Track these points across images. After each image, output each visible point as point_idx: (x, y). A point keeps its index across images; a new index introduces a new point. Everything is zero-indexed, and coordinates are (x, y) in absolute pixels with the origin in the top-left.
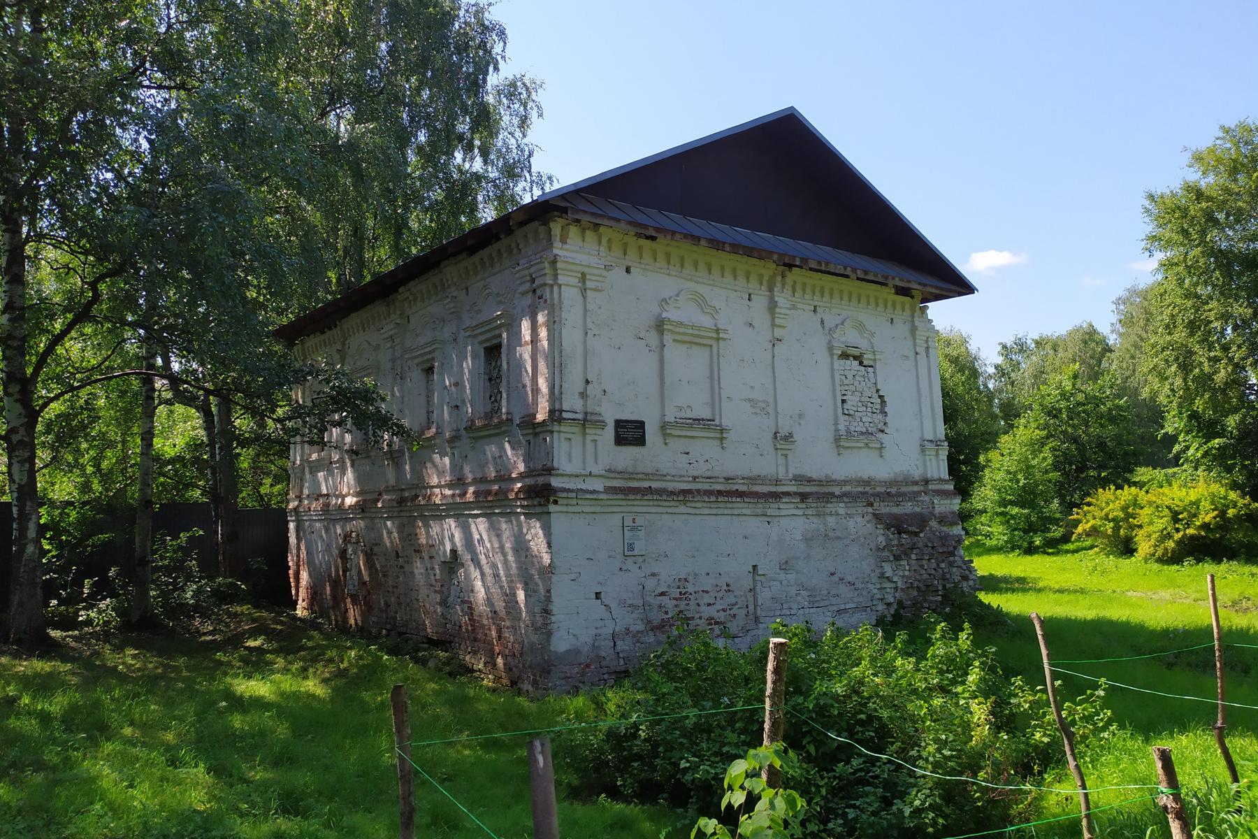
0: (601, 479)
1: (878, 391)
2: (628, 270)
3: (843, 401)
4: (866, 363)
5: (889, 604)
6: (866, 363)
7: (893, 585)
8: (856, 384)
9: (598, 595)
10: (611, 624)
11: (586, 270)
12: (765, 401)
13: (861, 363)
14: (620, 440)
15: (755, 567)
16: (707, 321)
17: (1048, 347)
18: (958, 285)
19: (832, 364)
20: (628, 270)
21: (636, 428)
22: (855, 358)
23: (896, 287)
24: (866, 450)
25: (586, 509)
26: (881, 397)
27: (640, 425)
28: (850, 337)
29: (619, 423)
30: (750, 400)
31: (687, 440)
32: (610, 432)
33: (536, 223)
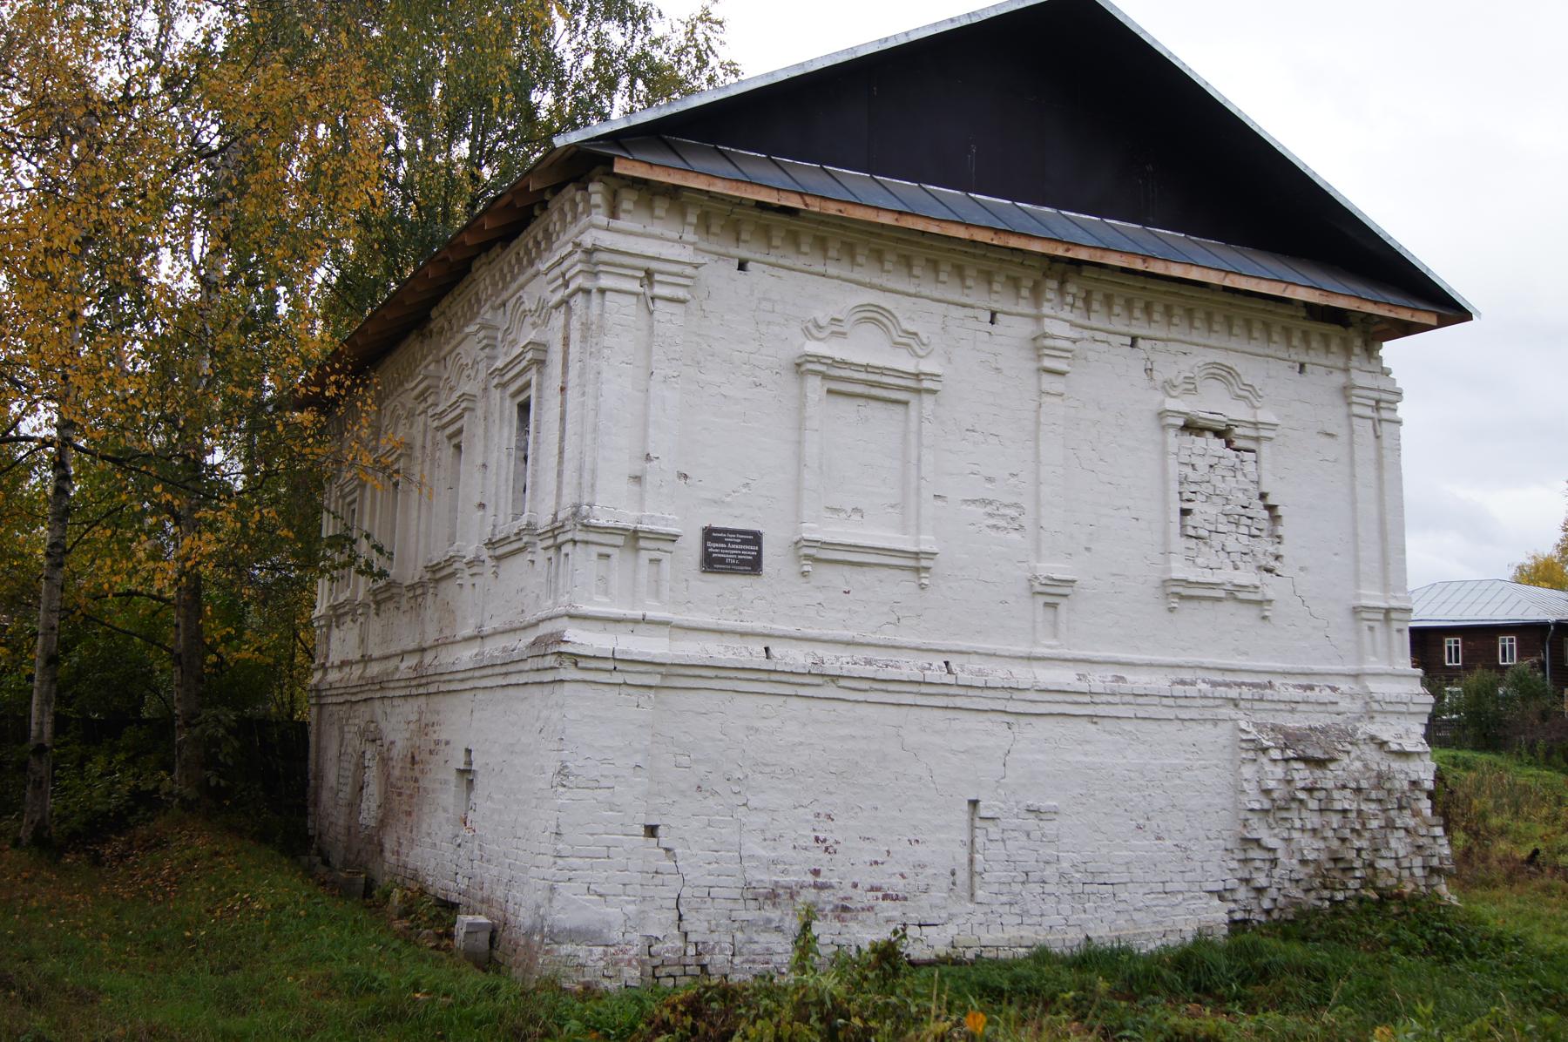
0: (759, 639)
1: (1263, 496)
2: (742, 266)
3: (1185, 512)
4: (1238, 443)
5: (1260, 891)
6: (1238, 443)
7: (1266, 855)
8: (1216, 480)
9: (651, 831)
10: (674, 883)
11: (653, 265)
12: (1016, 505)
13: (1229, 444)
14: (711, 563)
15: (974, 803)
16: (906, 363)
17: (1086, 1022)
18: (1451, 310)
19: (1165, 443)
20: (742, 266)
21: (744, 542)
22: (1218, 434)
23: (1470, 849)
24: (1229, 606)
25: (630, 679)
26: (1271, 508)
27: (755, 538)
28: (1214, 403)
29: (709, 534)
30: (985, 502)
31: (846, 568)
32: (692, 547)
33: (571, 188)
